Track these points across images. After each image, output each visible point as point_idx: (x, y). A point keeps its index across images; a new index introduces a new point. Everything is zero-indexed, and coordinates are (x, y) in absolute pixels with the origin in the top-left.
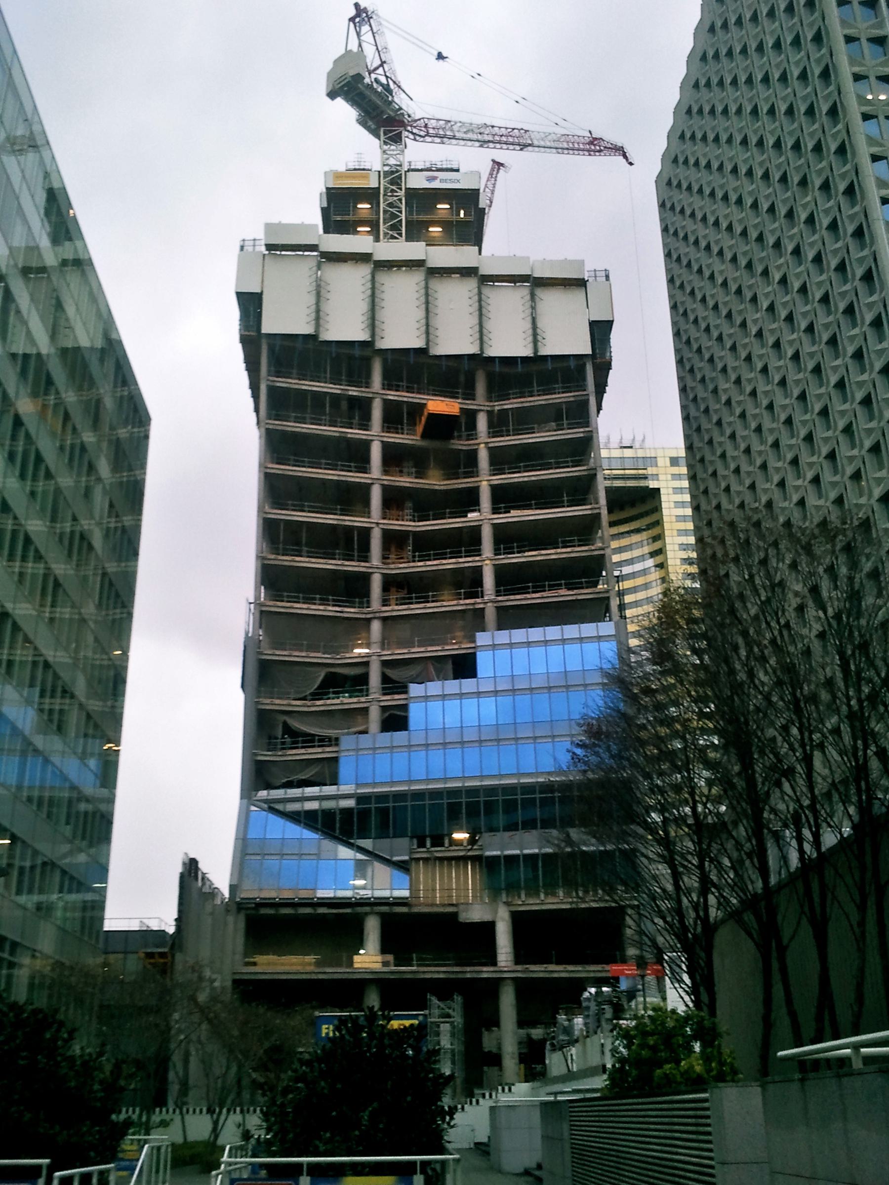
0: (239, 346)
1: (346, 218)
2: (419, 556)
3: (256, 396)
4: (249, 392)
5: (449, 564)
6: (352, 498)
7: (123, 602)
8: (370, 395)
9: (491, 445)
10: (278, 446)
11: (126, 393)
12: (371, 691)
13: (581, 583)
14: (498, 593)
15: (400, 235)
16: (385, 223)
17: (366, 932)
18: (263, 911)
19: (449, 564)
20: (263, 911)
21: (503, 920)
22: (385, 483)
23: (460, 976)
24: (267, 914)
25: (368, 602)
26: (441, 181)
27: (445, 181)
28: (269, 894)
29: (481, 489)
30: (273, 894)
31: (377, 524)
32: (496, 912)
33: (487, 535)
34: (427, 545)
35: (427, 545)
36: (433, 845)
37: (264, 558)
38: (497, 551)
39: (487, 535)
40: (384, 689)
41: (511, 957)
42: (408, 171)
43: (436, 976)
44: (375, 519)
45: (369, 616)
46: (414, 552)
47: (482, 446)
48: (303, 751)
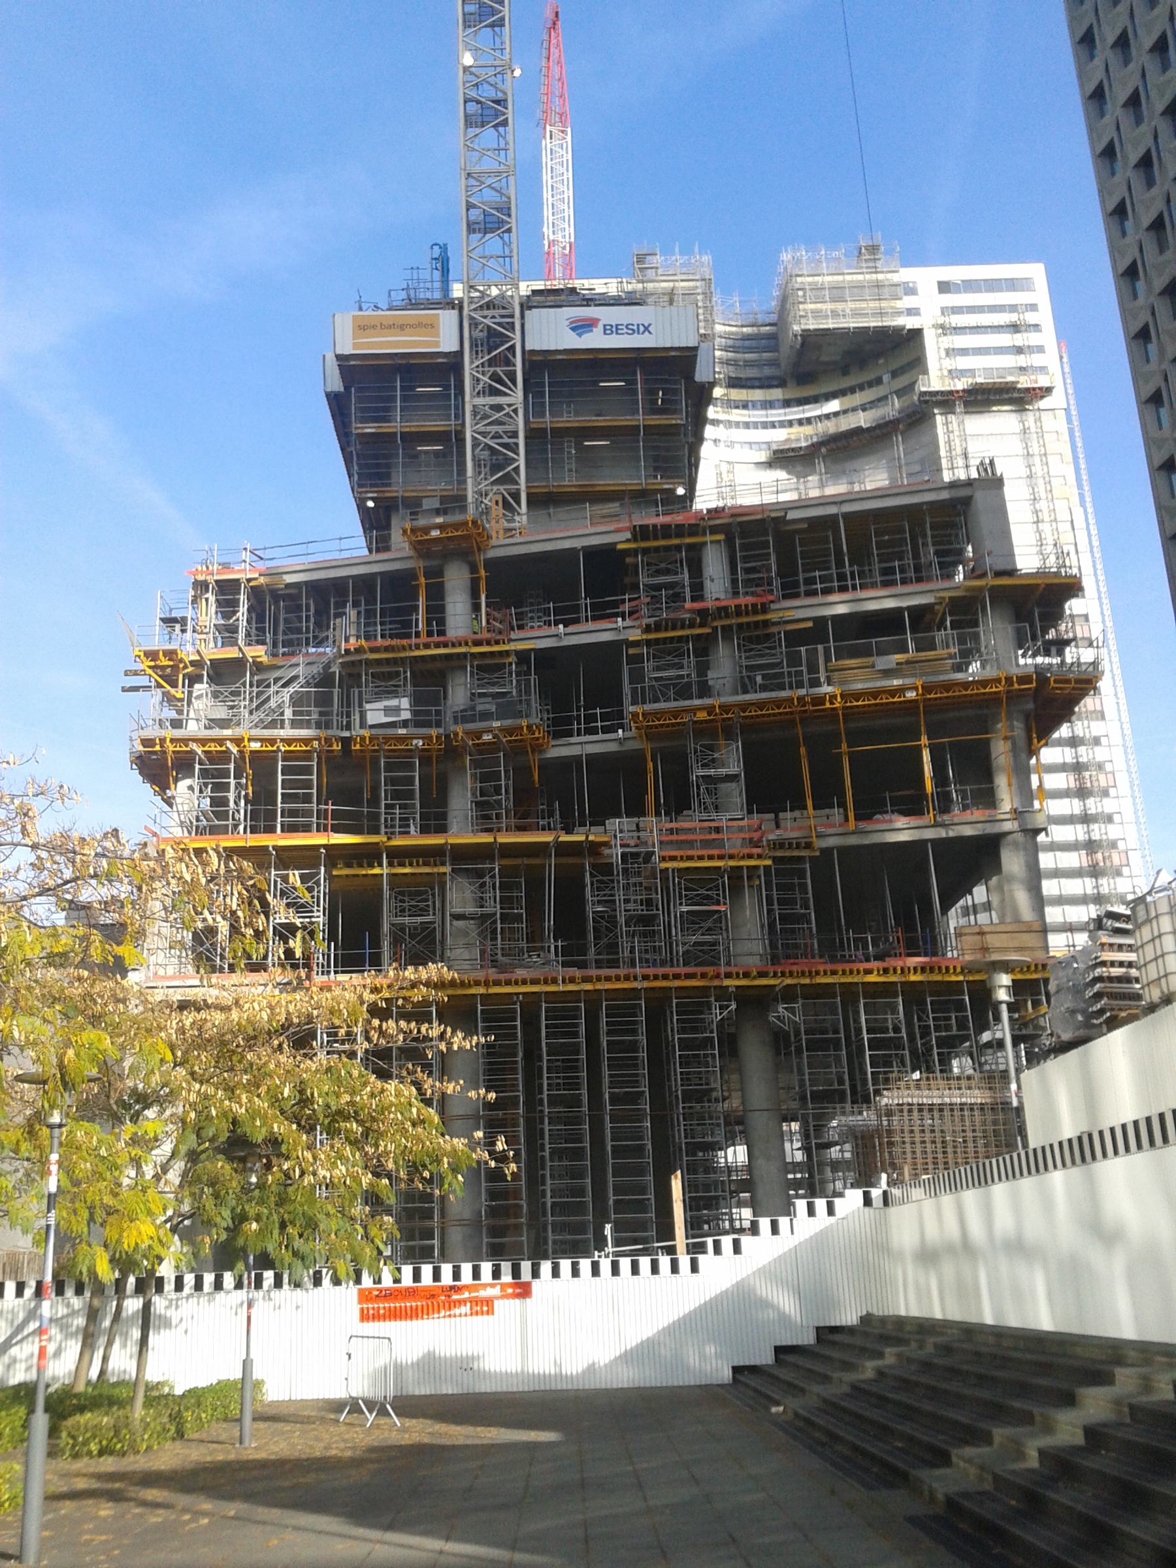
26: (609, 330)
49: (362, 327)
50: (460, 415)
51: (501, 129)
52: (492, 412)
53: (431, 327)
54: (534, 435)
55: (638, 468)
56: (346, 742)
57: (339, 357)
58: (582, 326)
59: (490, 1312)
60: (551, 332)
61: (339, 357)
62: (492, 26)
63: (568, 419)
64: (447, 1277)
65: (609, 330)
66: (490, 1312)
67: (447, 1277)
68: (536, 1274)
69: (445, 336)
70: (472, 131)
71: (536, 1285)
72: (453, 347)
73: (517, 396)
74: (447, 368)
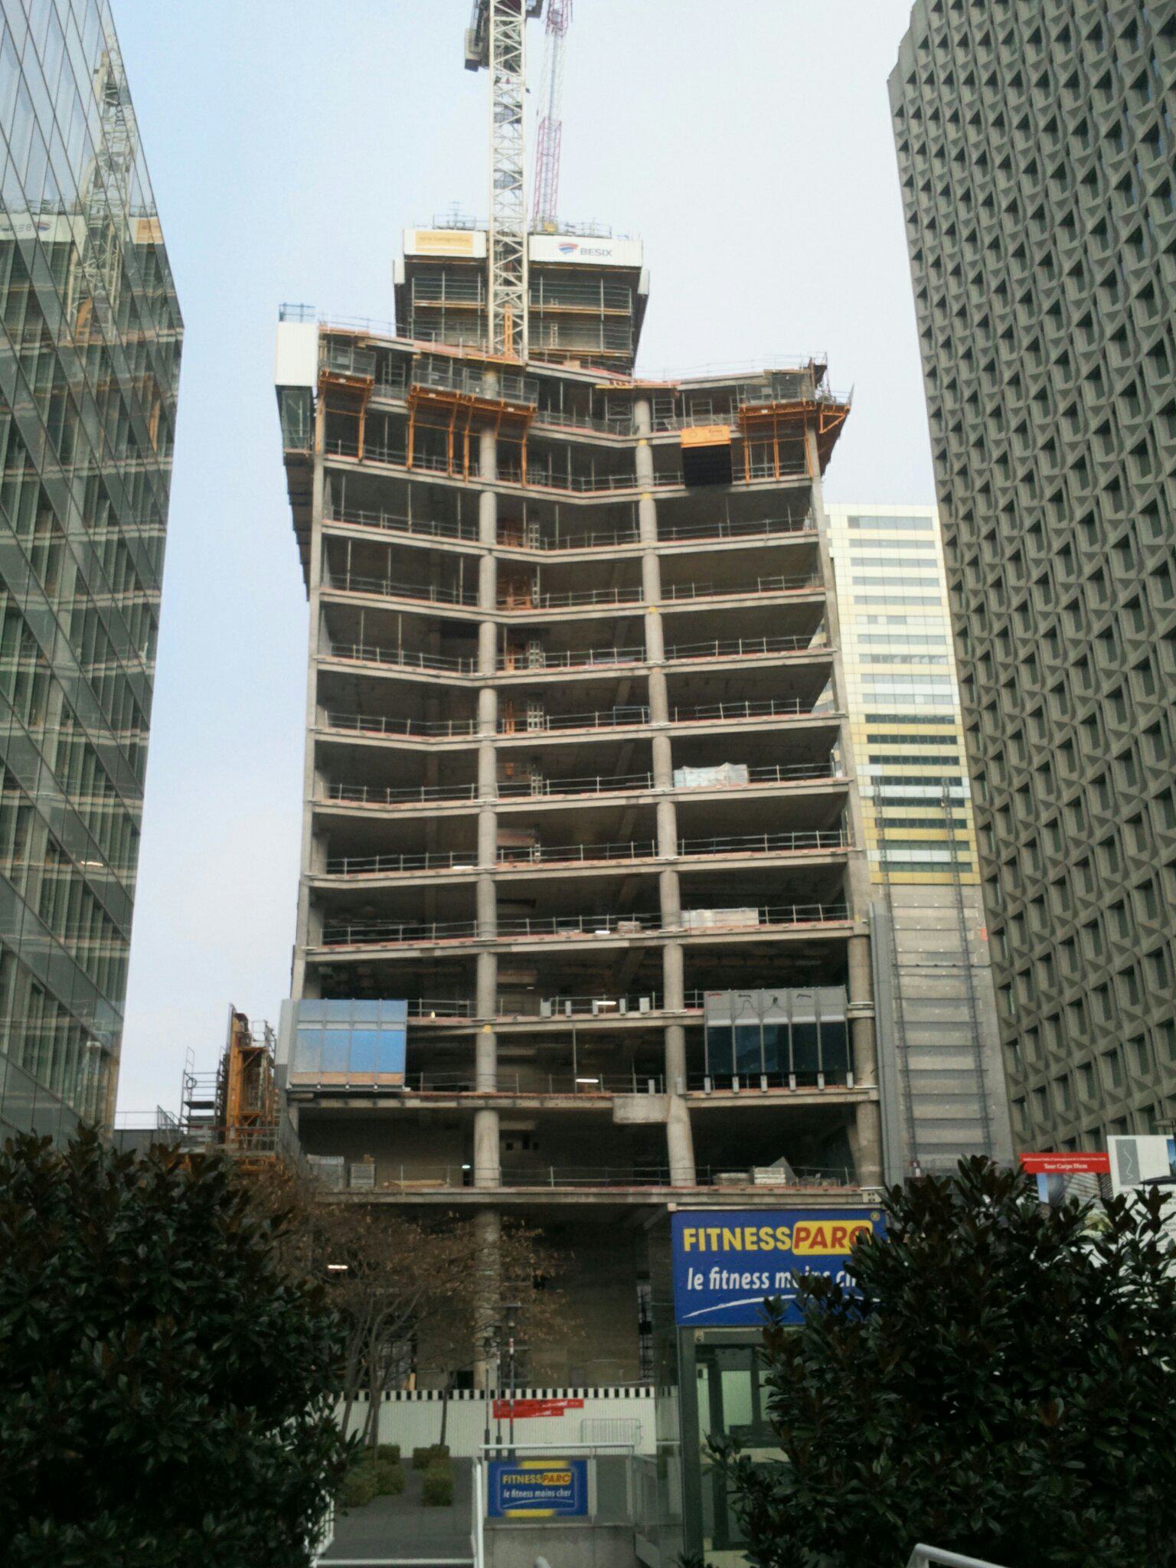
0: (283, 470)
1: (435, 304)
2: (552, 785)
3: (304, 543)
4: (293, 536)
5: (595, 611)
6: (453, 576)
7: (138, 451)
8: (478, 487)
9: (656, 442)
10: (338, 627)
11: (115, 537)
12: (482, 790)
13: (792, 641)
14: (668, 654)
15: (520, 279)
16: (497, 56)
17: (477, 1137)
18: (325, 1104)
19: (595, 611)
20: (325, 1104)
21: (679, 1120)
22: (502, 491)
23: (619, 1200)
24: (332, 1110)
25: (476, 664)
26: (584, 251)
27: (589, 252)
28: (337, 1078)
29: (642, 505)
30: (340, 1080)
31: (490, 550)
32: (668, 1110)
33: (651, 572)
34: (562, 584)
35: (562, 584)
36: (574, 1012)
37: (315, 804)
38: (666, 594)
39: (651, 572)
40: (501, 788)
41: (691, 1174)
42: (531, 234)
43: (583, 1200)
44: (487, 545)
45: (477, 684)
46: (543, 592)
47: (643, 443)
48: (382, 875)
49: (422, 238)
50: (485, 299)
51: (517, 192)
52: (508, 300)
53: (468, 241)
54: (534, 316)
55: (598, 336)
56: (499, 1451)
57: (407, 257)
58: (567, 248)
59: (562, 1414)
60: (545, 250)
61: (407, 257)
62: (512, 123)
63: (555, 307)
64: (539, 1396)
65: (584, 251)
66: (562, 1414)
67: (539, 1396)
68: (586, 1395)
69: (476, 248)
70: (498, 191)
71: (586, 1403)
72: (482, 254)
73: (523, 287)
74: (480, 267)
